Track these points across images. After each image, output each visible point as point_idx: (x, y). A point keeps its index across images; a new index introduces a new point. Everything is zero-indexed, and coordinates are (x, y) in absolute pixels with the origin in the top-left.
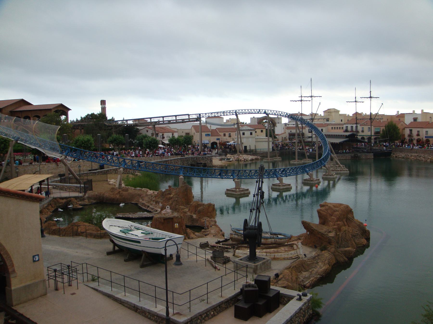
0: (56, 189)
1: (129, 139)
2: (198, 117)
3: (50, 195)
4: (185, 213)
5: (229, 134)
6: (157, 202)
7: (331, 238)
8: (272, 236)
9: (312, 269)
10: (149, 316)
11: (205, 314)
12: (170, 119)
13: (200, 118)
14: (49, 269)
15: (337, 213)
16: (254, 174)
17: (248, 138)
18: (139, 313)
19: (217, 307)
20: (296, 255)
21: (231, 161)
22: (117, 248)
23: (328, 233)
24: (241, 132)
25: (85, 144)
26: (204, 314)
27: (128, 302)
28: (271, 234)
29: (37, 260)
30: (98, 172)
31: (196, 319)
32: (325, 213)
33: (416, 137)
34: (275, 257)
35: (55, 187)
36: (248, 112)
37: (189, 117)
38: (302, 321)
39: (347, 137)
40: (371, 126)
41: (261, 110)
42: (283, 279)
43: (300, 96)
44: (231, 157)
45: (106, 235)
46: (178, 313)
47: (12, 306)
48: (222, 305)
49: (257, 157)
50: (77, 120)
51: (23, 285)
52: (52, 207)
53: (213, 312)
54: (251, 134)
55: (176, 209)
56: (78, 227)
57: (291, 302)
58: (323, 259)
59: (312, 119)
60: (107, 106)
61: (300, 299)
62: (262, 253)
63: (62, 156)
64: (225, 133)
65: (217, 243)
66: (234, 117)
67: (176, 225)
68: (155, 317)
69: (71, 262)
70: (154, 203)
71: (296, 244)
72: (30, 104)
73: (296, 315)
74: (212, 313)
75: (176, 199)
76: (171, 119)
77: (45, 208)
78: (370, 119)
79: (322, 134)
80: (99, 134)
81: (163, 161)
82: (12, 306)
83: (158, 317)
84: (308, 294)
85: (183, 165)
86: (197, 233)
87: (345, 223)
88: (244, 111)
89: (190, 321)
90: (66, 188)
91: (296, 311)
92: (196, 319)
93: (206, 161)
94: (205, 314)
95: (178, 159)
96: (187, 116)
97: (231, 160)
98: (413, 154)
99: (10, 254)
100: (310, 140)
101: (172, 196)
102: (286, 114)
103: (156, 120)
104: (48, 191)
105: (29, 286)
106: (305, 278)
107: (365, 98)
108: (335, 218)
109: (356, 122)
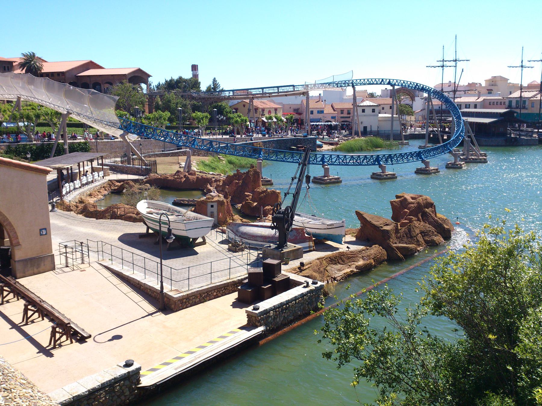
5: (363, 109)
9: (353, 263)
12: (286, 89)
14: (61, 245)
22: (151, 231)
23: (384, 226)
26: (204, 293)
29: (44, 234)
30: (173, 153)
31: (194, 297)
35: (114, 169)
36: (368, 82)
41: (384, 80)
52: (106, 190)
54: (373, 111)
56: (118, 210)
74: (215, 294)
79: (103, 91)
80: (215, 109)
88: (362, 81)
90: (126, 169)
92: (194, 297)
96: (276, 89)
99: (14, 226)
102: (415, 84)
103: (254, 92)
109: (520, 95)
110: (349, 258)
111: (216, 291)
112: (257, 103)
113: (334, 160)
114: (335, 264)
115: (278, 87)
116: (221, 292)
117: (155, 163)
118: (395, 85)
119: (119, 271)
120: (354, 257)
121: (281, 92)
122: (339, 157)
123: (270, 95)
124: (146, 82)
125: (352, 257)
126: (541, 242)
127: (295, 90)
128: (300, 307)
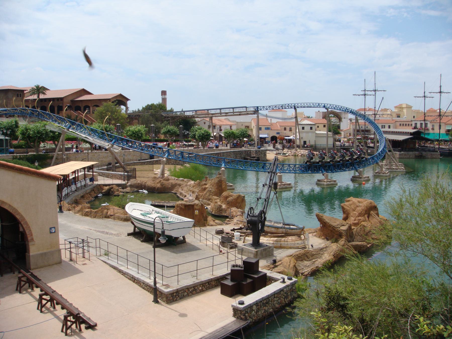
0: (102, 176)
1: (184, 131)
2: (255, 110)
3: (94, 182)
7: (342, 231)
8: (284, 226)
9: (316, 259)
10: (143, 286)
11: (193, 289)
13: (258, 111)
15: (360, 208)
17: (307, 132)
18: (136, 283)
19: (206, 283)
20: (303, 245)
21: (287, 156)
23: (341, 226)
24: (300, 127)
25: (135, 134)
26: (191, 288)
27: (128, 273)
28: (283, 224)
29: (53, 232)
30: (148, 162)
31: (182, 291)
32: (348, 208)
34: (282, 245)
37: (246, 110)
38: (283, 302)
39: (411, 134)
40: (440, 123)
42: (281, 265)
43: (364, 90)
44: (288, 152)
45: (128, 219)
47: (30, 269)
48: (212, 283)
49: (38, 171)
50: (139, 110)
51: (41, 252)
53: (202, 287)
54: (311, 128)
55: (209, 199)
58: (329, 251)
59: (375, 114)
60: (168, 96)
61: (284, 282)
62: (269, 241)
63: (109, 145)
64: (416, 122)
65: (232, 230)
68: (148, 287)
72: (90, 93)
73: (274, 295)
74: (200, 288)
75: (210, 189)
76: (228, 112)
77: (87, 194)
80: (181, 126)
81: (215, 153)
82: (30, 269)
83: (150, 287)
84: (293, 278)
85: (236, 158)
86: (217, 221)
87: (367, 218)
89: (176, 293)
91: (275, 292)
92: (182, 291)
93: (260, 154)
94: (193, 289)
95: (231, 151)
96: (245, 108)
97: (287, 155)
101: (207, 186)
102: (345, 108)
103: (213, 112)
104: (93, 177)
105: (45, 254)
106: (305, 266)
108: (357, 214)
110: (313, 255)
112: (216, 120)
113: (285, 168)
114: (302, 260)
115: (233, 108)
116: (206, 287)
117: (135, 170)
118: (329, 108)
119: (116, 266)
120: (317, 254)
121: (223, 113)
122: (290, 166)
123: (226, 114)
124: (125, 105)
125: (316, 254)
127: (248, 110)
128: (278, 300)
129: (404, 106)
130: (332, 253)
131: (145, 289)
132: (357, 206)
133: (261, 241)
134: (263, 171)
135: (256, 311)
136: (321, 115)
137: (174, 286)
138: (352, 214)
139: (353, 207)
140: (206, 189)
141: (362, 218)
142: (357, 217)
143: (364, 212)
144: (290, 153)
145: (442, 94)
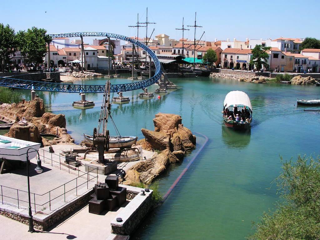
4: (39, 123)
5: (231, 56)
6: (12, 114)
9: (151, 169)
16: (98, 89)
17: (90, 57)
19: (73, 205)
32: (160, 123)
33: (230, 61)
34: (120, 159)
39: (174, 58)
46: (39, 213)
57: (137, 197)
59: (146, 42)
61: (144, 194)
66: (80, 38)
67: (32, 134)
68: (18, 217)
69: (2, 186)
70: (9, 115)
71: (137, 149)
75: (30, 111)
78: (194, 45)
84: (150, 190)
98: (227, 74)
100: (144, 60)
102: (124, 37)
107: (142, 23)
111: (70, 208)
120: (150, 165)
126: (1, 120)
129: (163, 36)
130: (162, 162)
131: (14, 219)
132: (168, 121)
133: (105, 158)
134: (69, 91)
135: (130, 225)
136: (98, 42)
137: (49, 212)
138: (163, 127)
139: (164, 122)
140: (25, 110)
141: (173, 130)
142: (168, 130)
143: (174, 125)
144: (78, 75)
145: (197, 28)
